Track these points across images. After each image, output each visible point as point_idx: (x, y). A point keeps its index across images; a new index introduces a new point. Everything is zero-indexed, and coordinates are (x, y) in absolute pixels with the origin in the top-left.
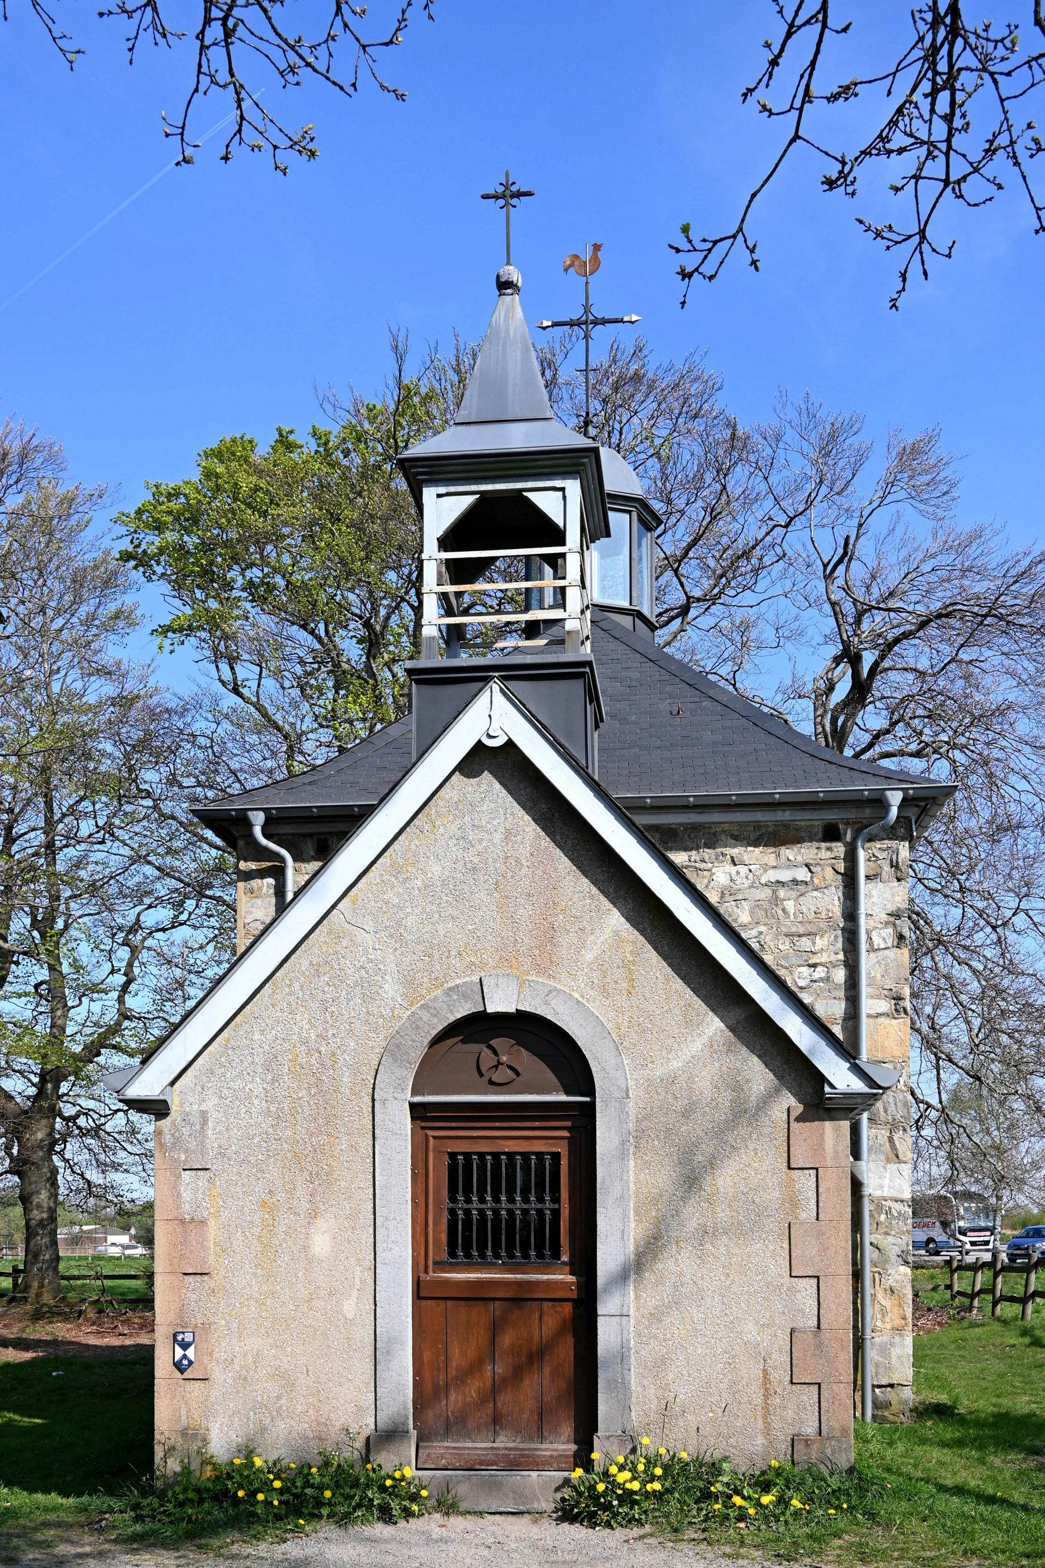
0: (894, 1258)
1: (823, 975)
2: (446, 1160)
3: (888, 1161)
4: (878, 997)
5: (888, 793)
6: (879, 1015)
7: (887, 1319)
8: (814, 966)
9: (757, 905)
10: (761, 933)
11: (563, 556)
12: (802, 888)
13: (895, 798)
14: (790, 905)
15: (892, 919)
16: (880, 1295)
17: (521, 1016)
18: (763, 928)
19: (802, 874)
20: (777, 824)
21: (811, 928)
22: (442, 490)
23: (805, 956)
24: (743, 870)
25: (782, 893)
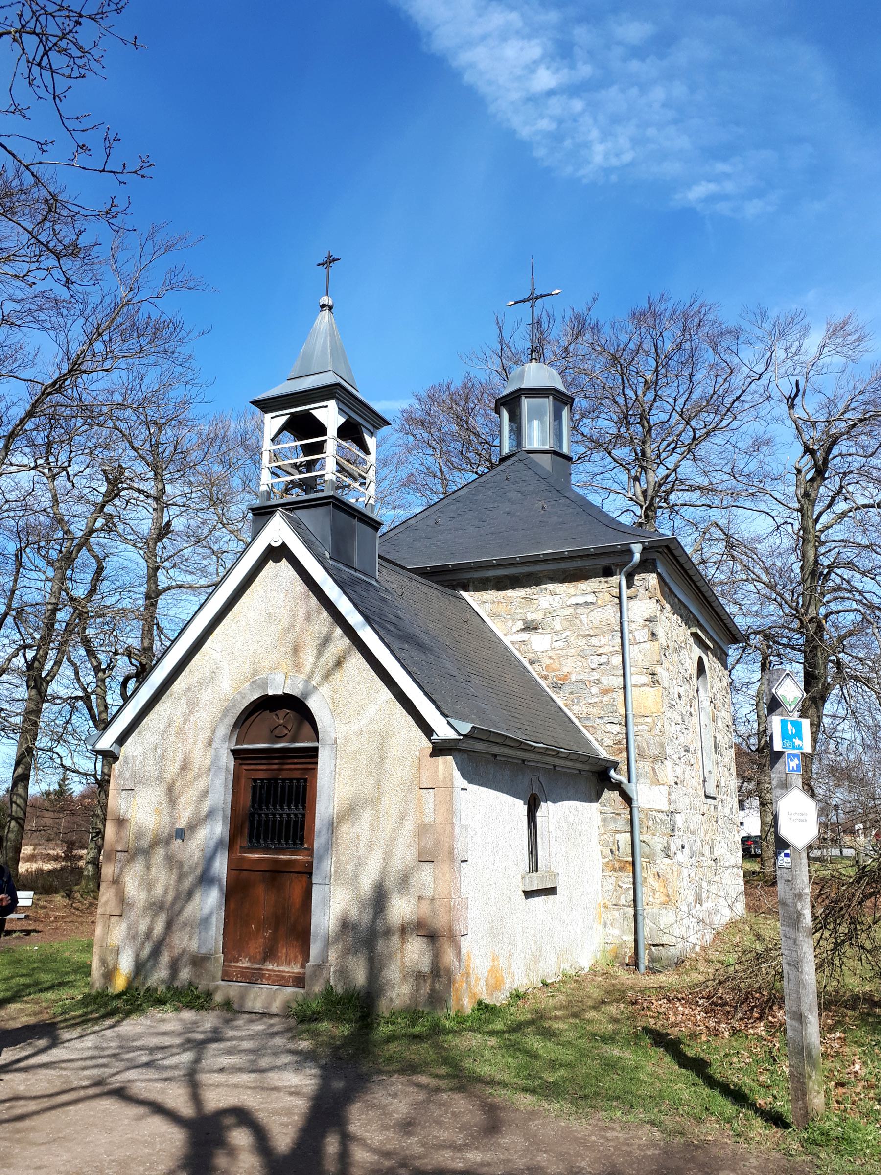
0: (659, 853)
1: (605, 660)
2: (251, 784)
3: (652, 784)
4: (641, 674)
5: (632, 546)
6: (641, 685)
7: (657, 896)
8: (600, 655)
9: (566, 618)
10: (567, 636)
11: (325, 441)
12: (591, 607)
13: (637, 549)
14: (584, 618)
15: (647, 623)
16: (651, 879)
17: (286, 696)
18: (568, 633)
19: (591, 598)
20: (576, 569)
21: (598, 631)
22: (273, 414)
23: (595, 649)
24: (557, 598)
25: (580, 610)
